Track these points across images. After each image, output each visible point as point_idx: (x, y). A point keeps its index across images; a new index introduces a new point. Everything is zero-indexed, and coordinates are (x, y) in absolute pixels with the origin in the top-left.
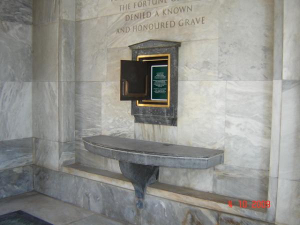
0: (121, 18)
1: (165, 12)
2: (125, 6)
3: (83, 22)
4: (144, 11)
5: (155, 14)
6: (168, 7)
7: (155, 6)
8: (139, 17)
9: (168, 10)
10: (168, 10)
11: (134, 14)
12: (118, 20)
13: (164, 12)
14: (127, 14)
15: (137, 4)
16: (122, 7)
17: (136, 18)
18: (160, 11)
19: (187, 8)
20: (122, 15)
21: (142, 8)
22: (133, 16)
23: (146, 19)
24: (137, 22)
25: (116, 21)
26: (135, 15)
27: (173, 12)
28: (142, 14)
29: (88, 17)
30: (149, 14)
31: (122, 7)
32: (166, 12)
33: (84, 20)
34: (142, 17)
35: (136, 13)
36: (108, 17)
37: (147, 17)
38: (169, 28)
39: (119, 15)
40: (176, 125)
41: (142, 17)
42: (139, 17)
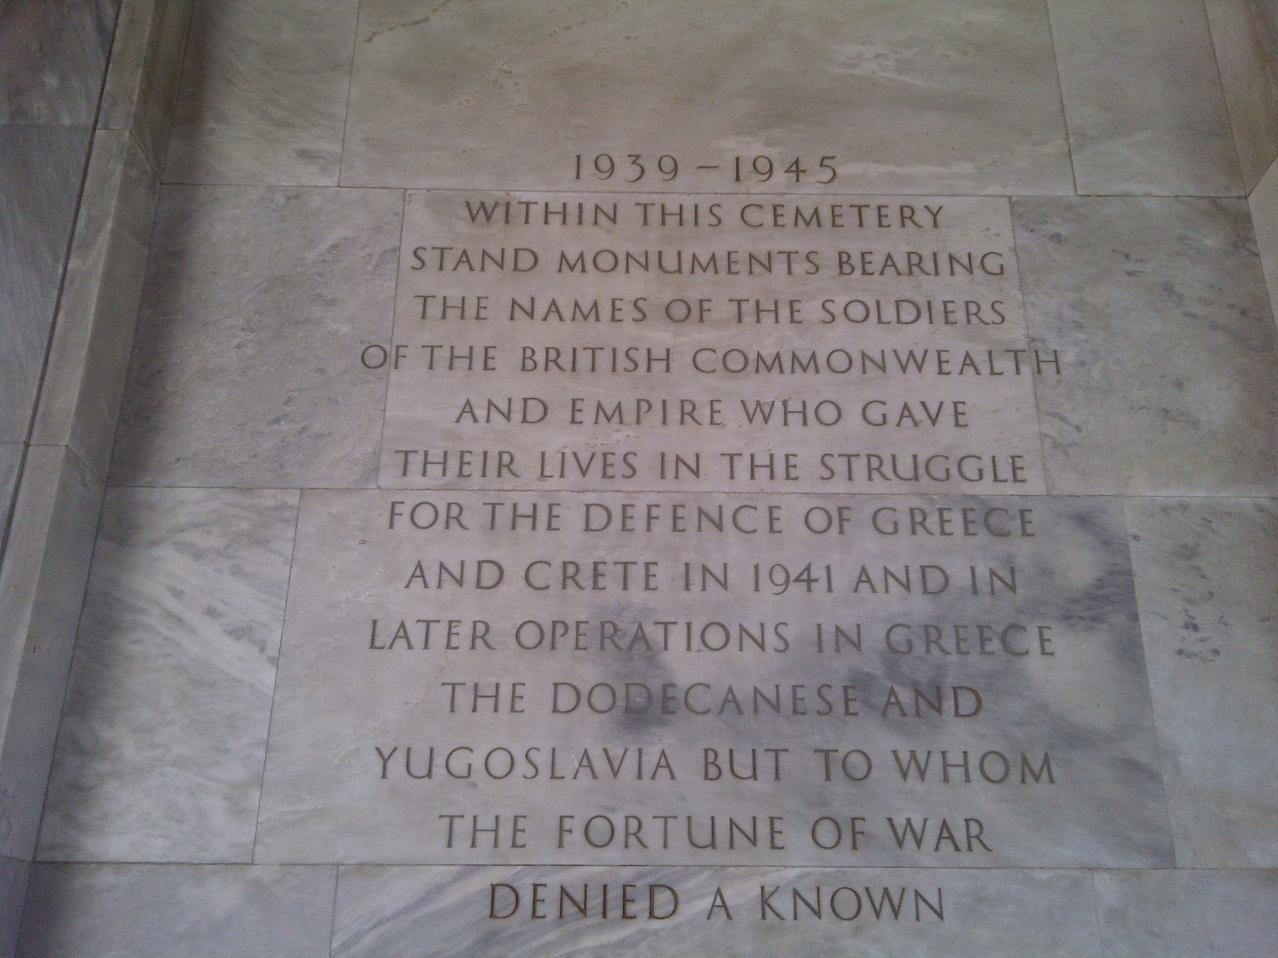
0: (453, 897)
1: (776, 902)
2: (486, 822)
3: (105, 878)
4: (626, 874)
5: (705, 903)
6: (791, 873)
7: (707, 856)
8: (595, 903)
9: (796, 893)
10: (796, 893)
11: (554, 881)
12: (424, 900)
13: (765, 901)
14: (497, 875)
15: (577, 826)
16: (463, 827)
17: (569, 909)
18: (742, 894)
19: (910, 898)
20: (457, 879)
21: (613, 854)
22: (550, 895)
23: (643, 923)
24: (577, 935)
25: (408, 909)
26: (563, 891)
27: (734, 632)
28: (615, 894)
29: (157, 849)
30: (663, 897)
31: (463, 827)
32: (783, 904)
33: (119, 865)
34: (614, 913)
35: (566, 878)
36: (338, 871)
37: (651, 915)
38: (493, 453)
39: (437, 874)
40: (915, 716)
41: (614, 913)
42: (595, 903)
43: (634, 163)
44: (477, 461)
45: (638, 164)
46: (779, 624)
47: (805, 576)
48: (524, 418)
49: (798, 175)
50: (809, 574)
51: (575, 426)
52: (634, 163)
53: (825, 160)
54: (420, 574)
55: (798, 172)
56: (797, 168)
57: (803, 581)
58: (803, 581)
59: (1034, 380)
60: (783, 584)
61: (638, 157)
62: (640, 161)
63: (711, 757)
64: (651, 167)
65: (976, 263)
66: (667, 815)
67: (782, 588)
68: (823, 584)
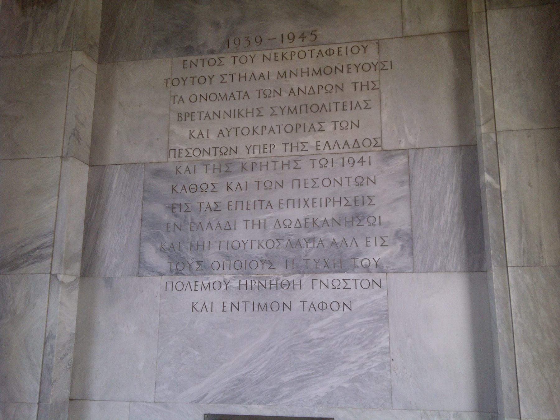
43: (247, 40)
44: (318, 201)
45: (248, 40)
46: (355, 180)
47: (361, 161)
48: (307, 106)
49: (303, 39)
50: (362, 160)
51: (345, 111)
52: (247, 40)
53: (313, 32)
54: (205, 307)
55: (303, 38)
56: (303, 36)
57: (361, 162)
58: (361, 162)
59: (471, 72)
60: (352, 164)
61: (248, 37)
62: (249, 39)
63: (180, 115)
64: (252, 40)
65: (334, 71)
66: (216, 147)
67: (352, 165)
68: (368, 162)
